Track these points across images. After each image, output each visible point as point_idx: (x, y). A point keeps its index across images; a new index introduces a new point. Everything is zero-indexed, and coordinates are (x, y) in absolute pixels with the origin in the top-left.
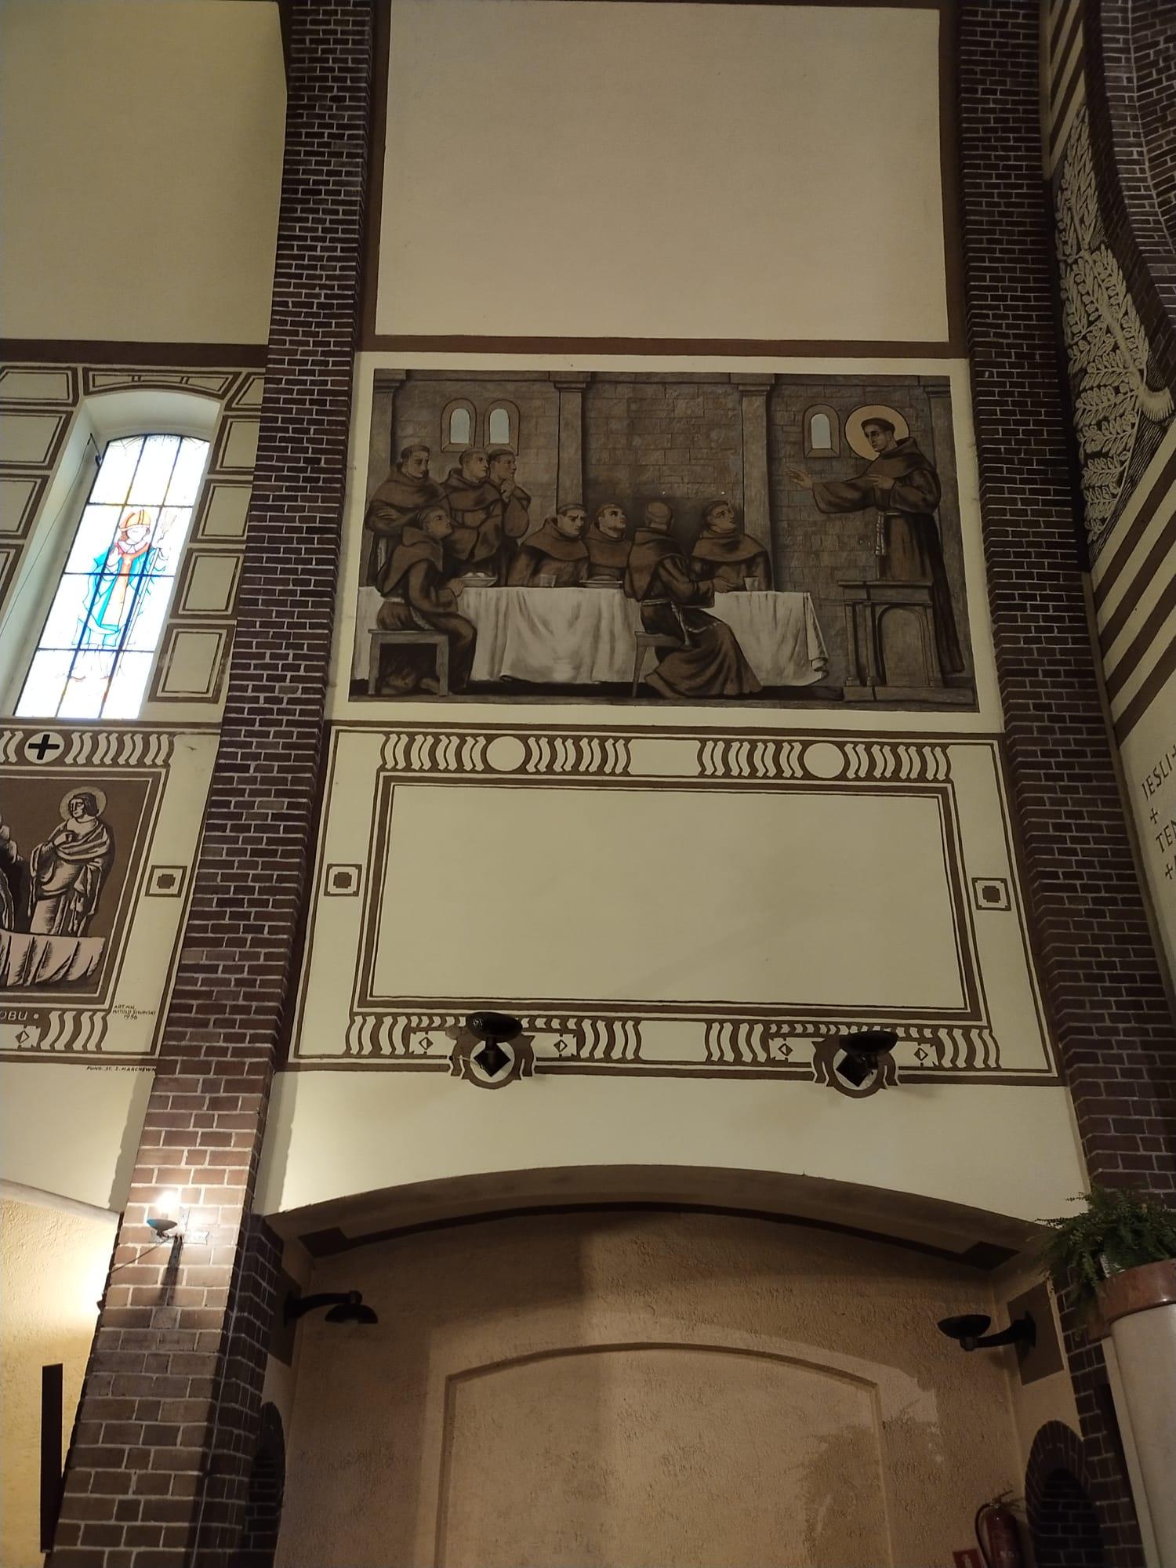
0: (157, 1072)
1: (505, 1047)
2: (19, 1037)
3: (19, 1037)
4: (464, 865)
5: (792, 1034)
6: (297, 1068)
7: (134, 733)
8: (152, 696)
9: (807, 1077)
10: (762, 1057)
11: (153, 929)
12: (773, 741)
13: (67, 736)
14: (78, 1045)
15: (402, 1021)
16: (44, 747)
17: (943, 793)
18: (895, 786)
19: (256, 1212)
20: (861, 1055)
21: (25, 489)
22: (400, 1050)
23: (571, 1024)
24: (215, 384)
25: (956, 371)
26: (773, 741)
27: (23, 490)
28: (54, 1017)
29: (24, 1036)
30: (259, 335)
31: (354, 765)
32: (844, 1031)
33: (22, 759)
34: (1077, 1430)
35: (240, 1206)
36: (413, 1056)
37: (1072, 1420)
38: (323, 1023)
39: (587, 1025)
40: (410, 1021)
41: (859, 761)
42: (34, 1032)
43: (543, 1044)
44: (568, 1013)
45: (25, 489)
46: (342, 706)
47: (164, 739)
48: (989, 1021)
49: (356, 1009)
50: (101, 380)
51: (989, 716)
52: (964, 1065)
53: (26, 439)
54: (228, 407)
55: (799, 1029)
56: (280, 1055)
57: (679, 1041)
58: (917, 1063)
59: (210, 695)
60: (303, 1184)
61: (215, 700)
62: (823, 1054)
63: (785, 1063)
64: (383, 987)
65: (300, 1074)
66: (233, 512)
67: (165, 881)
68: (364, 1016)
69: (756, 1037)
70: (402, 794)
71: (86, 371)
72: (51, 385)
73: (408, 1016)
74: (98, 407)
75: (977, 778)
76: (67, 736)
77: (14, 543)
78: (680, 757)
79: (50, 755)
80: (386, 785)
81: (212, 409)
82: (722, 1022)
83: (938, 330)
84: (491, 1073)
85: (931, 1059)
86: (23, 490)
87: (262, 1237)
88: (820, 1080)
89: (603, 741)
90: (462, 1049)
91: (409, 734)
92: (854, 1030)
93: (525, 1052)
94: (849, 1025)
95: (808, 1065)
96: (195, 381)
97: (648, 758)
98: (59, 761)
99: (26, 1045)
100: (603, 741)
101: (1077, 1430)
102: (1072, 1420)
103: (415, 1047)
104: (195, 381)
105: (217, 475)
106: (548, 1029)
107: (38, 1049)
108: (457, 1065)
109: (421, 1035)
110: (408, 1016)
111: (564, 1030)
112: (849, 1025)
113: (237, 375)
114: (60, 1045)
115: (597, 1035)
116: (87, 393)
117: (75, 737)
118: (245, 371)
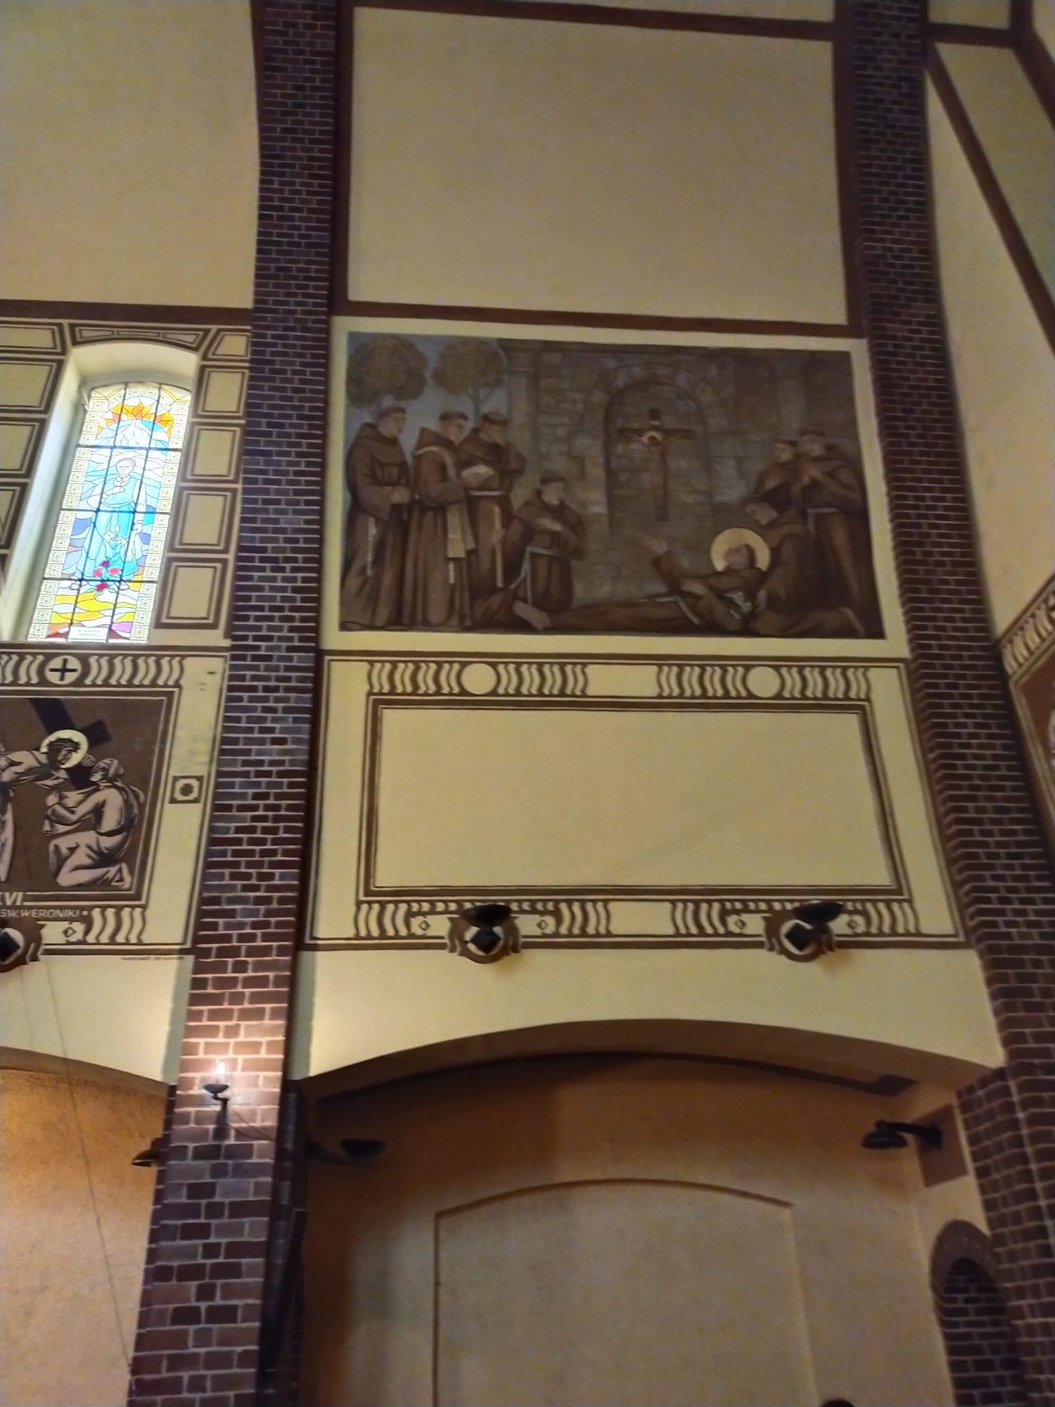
0: (197, 958)
1: (498, 930)
2: (65, 932)
3: (65, 932)
4: (457, 771)
5: (746, 910)
6: (315, 948)
7: (101, 656)
8: (158, 624)
9: (760, 945)
10: (403, 932)
11: (179, 835)
12: (720, 666)
13: (84, 660)
14: (120, 938)
15: (403, 907)
16: (64, 670)
17: (861, 709)
18: (824, 705)
19: (297, 1075)
20: (811, 926)
21: (24, 432)
22: (403, 932)
23: (550, 906)
24: (189, 338)
25: (857, 350)
26: (720, 666)
27: (22, 433)
28: (96, 913)
29: (70, 932)
30: (244, 298)
31: (348, 689)
32: (789, 906)
33: (43, 681)
34: (983, 1226)
35: (279, 1074)
36: (729, 934)
37: (977, 1217)
38: (334, 911)
39: (563, 907)
40: (410, 907)
41: (793, 681)
42: (79, 927)
43: (527, 925)
44: (550, 898)
45: (24, 432)
46: (334, 637)
47: (175, 662)
48: (910, 894)
49: (362, 898)
50: (88, 333)
51: (896, 640)
52: (106, 941)
53: (20, 385)
54: (204, 358)
55: (440, 907)
56: (300, 938)
57: (628, 918)
58: (538, 932)
59: (210, 621)
60: (328, 1050)
61: (214, 626)
62: (772, 926)
63: (424, 937)
64: (385, 878)
65: (319, 953)
66: (220, 453)
67: (187, 790)
68: (369, 903)
69: (710, 915)
70: (392, 718)
71: (72, 326)
72: (38, 337)
73: (408, 902)
74: (83, 358)
75: (889, 696)
76: (84, 660)
77: (18, 483)
78: (641, 682)
79: (70, 677)
80: (379, 703)
81: (187, 362)
82: (685, 902)
83: (838, 315)
84: (800, 948)
85: (550, 929)
86: (22, 433)
87: (303, 1098)
88: (453, 950)
89: (540, 665)
90: (456, 933)
91: (721, 666)
92: (797, 904)
93: (512, 931)
94: (791, 901)
95: (442, 938)
96: (171, 336)
97: (602, 681)
98: (79, 682)
99: (73, 939)
100: (540, 665)
101: (983, 1226)
102: (977, 1217)
103: (417, 930)
104: (171, 336)
105: (203, 419)
106: (534, 911)
107: (84, 942)
108: (455, 942)
109: (421, 918)
110: (408, 902)
111: (545, 912)
112: (791, 901)
113: (207, 332)
114: (105, 938)
115: (575, 915)
116: (76, 343)
117: (93, 660)
118: (214, 328)
